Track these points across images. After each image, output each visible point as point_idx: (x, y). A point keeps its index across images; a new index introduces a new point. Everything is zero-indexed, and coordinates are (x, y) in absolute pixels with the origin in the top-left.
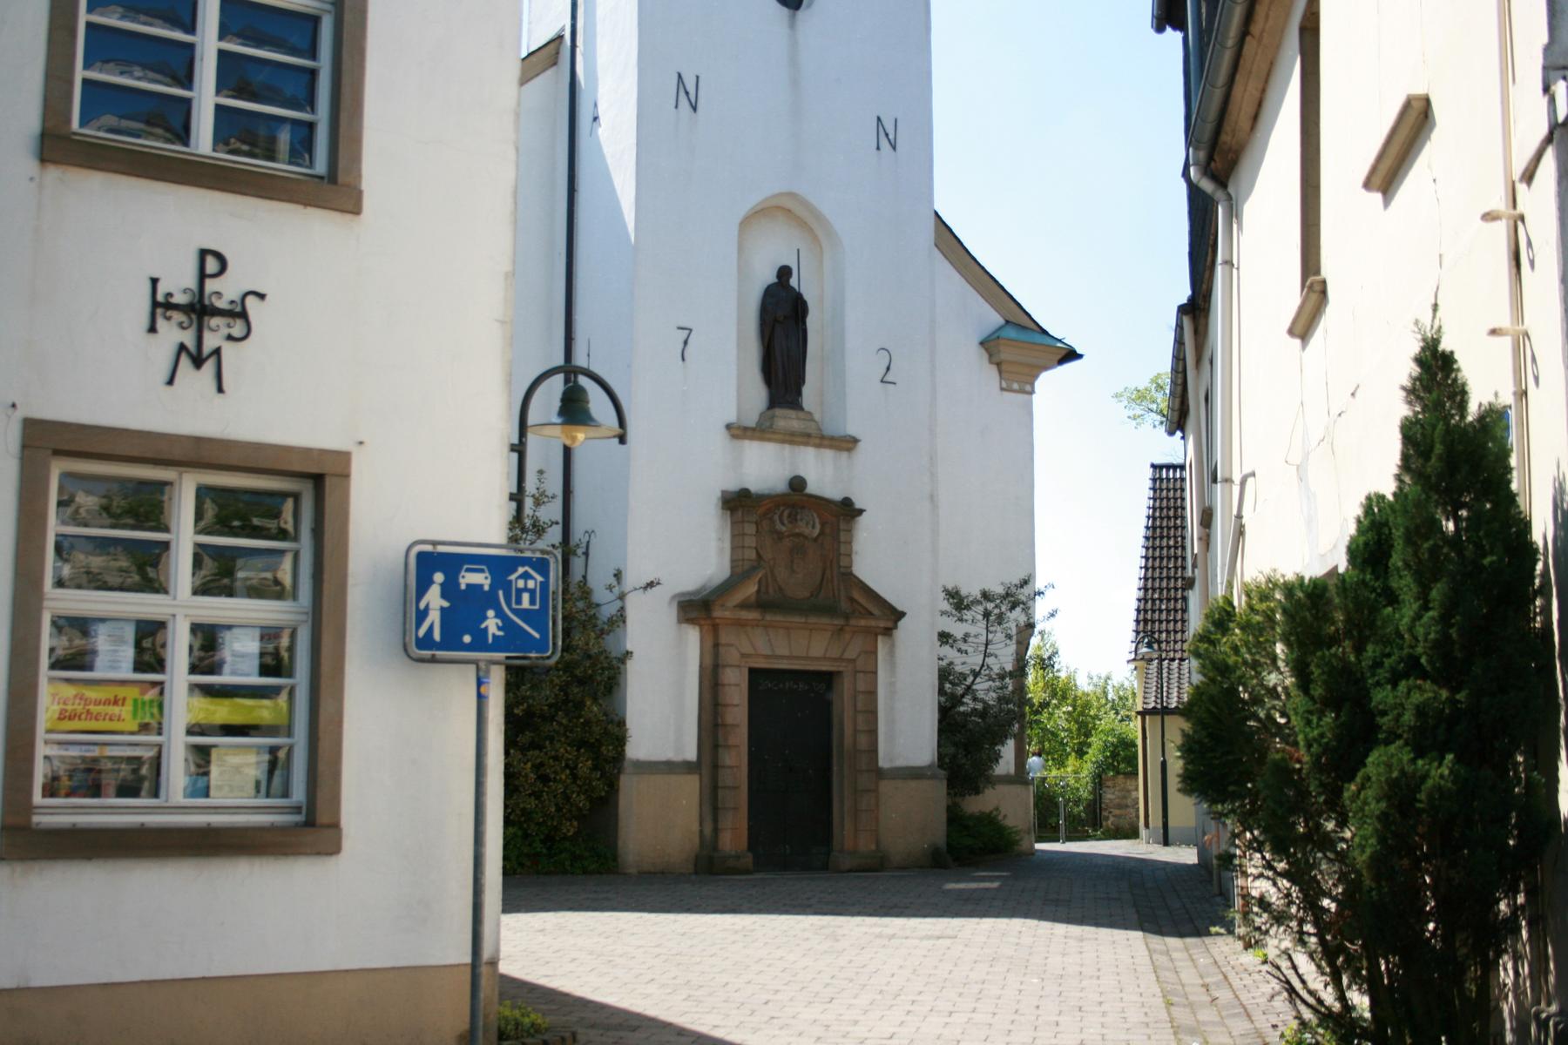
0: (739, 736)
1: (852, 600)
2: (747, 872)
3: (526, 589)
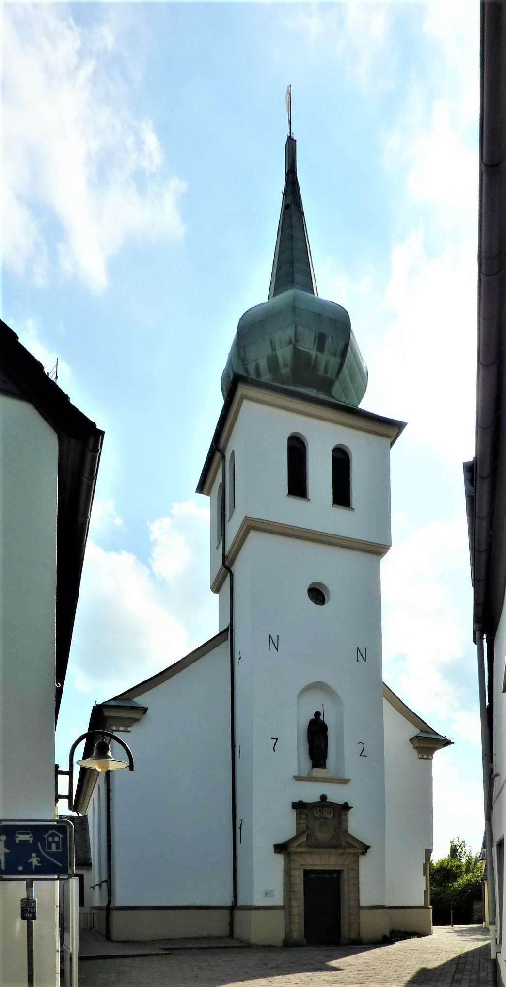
0: (301, 895)
1: (347, 842)
2: (303, 946)
3: (54, 842)
